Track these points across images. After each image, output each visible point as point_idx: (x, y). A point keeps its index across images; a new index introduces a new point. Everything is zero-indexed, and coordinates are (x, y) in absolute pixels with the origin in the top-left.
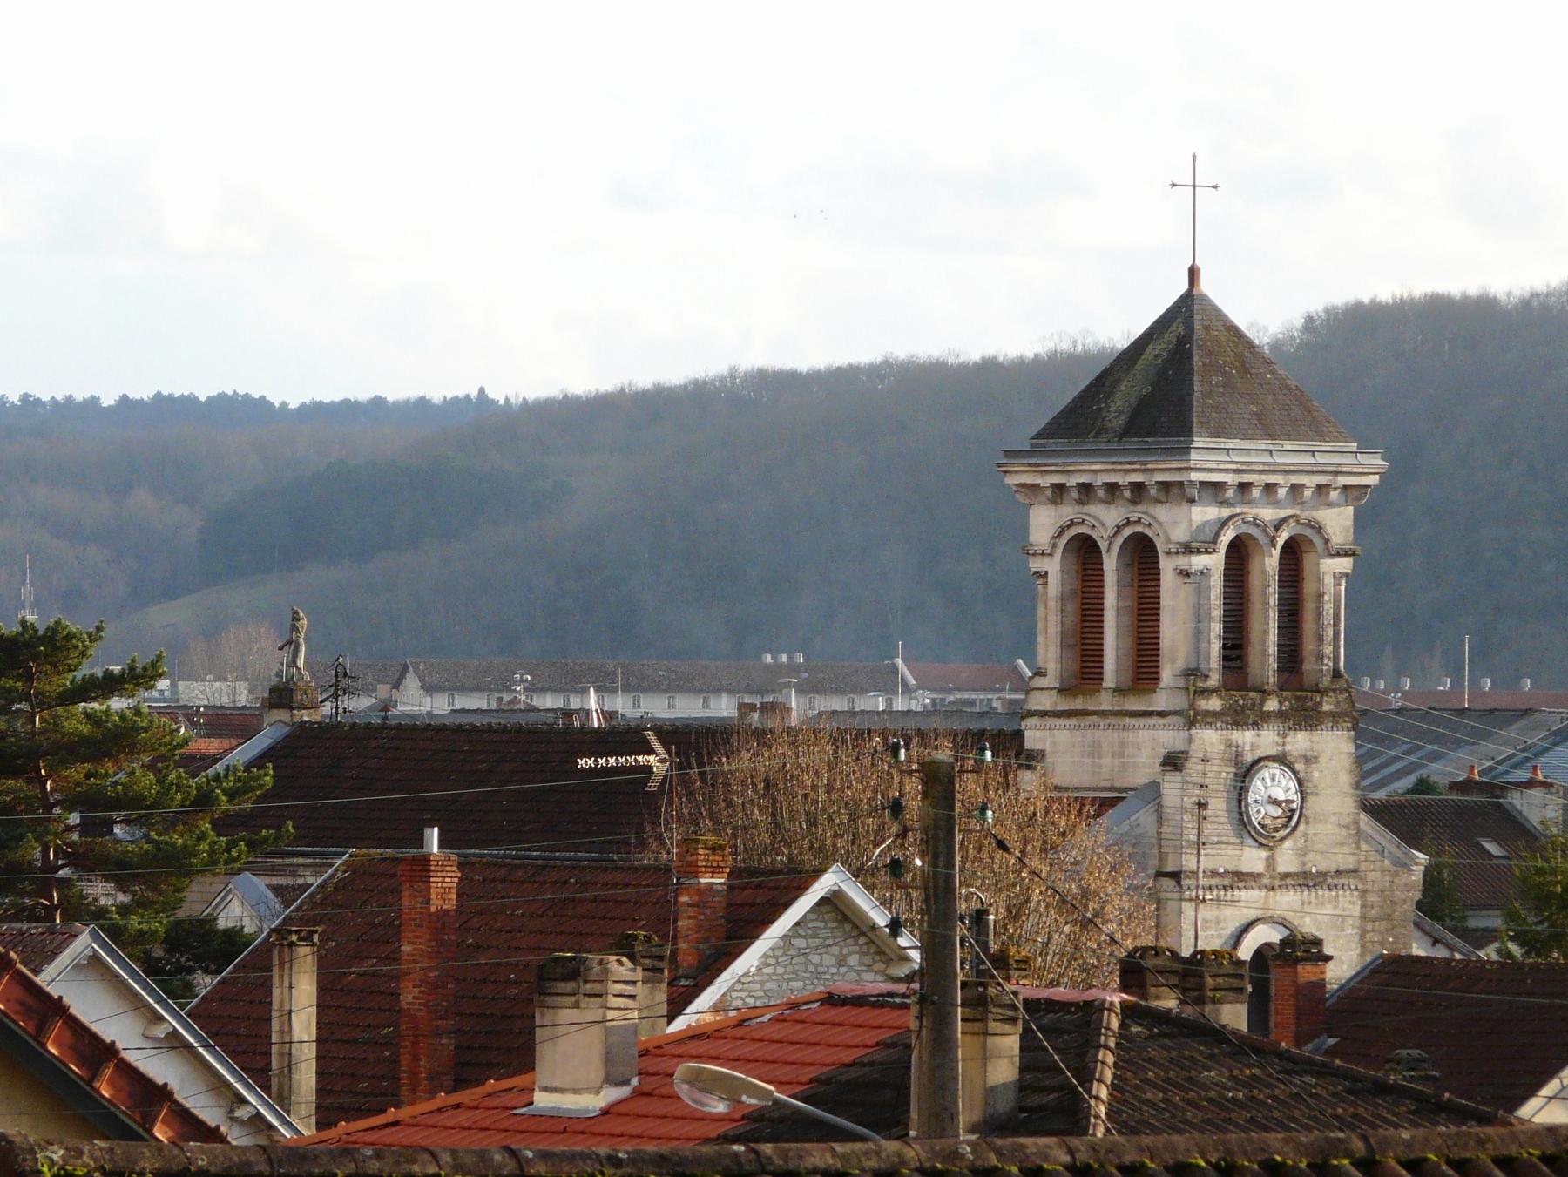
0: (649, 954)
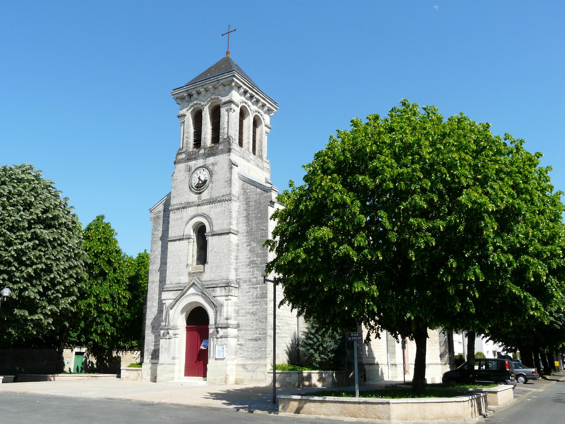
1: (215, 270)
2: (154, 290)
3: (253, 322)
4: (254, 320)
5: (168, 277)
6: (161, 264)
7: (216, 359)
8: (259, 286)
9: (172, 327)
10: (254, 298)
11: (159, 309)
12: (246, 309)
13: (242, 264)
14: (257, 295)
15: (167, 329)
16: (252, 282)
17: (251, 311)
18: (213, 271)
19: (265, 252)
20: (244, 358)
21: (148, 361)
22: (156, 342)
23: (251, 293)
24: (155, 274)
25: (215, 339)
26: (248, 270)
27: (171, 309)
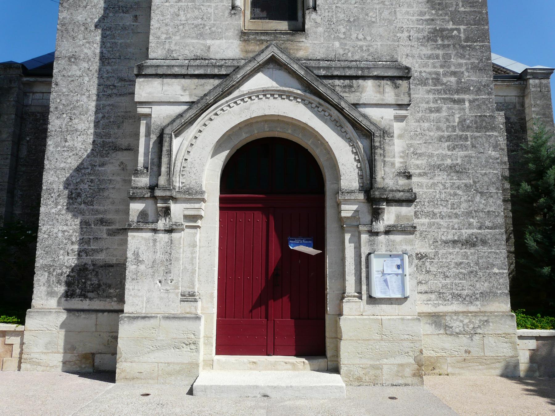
0: (155, 169)
1: (343, 30)
2: (76, 83)
3: (455, 194)
4: (458, 188)
5: (159, 38)
6: (105, 9)
7: (372, 300)
8: (466, 97)
9: (185, 192)
10: (453, 127)
11: (100, 140)
12: (431, 156)
13: (406, 34)
14: (465, 120)
15: (166, 199)
16: (443, 84)
17: (449, 162)
18: (337, 31)
19: (480, 13)
20: (433, 296)
21: (53, 303)
22: (88, 242)
23: (444, 114)
24: (81, 36)
25: (364, 237)
26: (430, 52)
27: (178, 133)
